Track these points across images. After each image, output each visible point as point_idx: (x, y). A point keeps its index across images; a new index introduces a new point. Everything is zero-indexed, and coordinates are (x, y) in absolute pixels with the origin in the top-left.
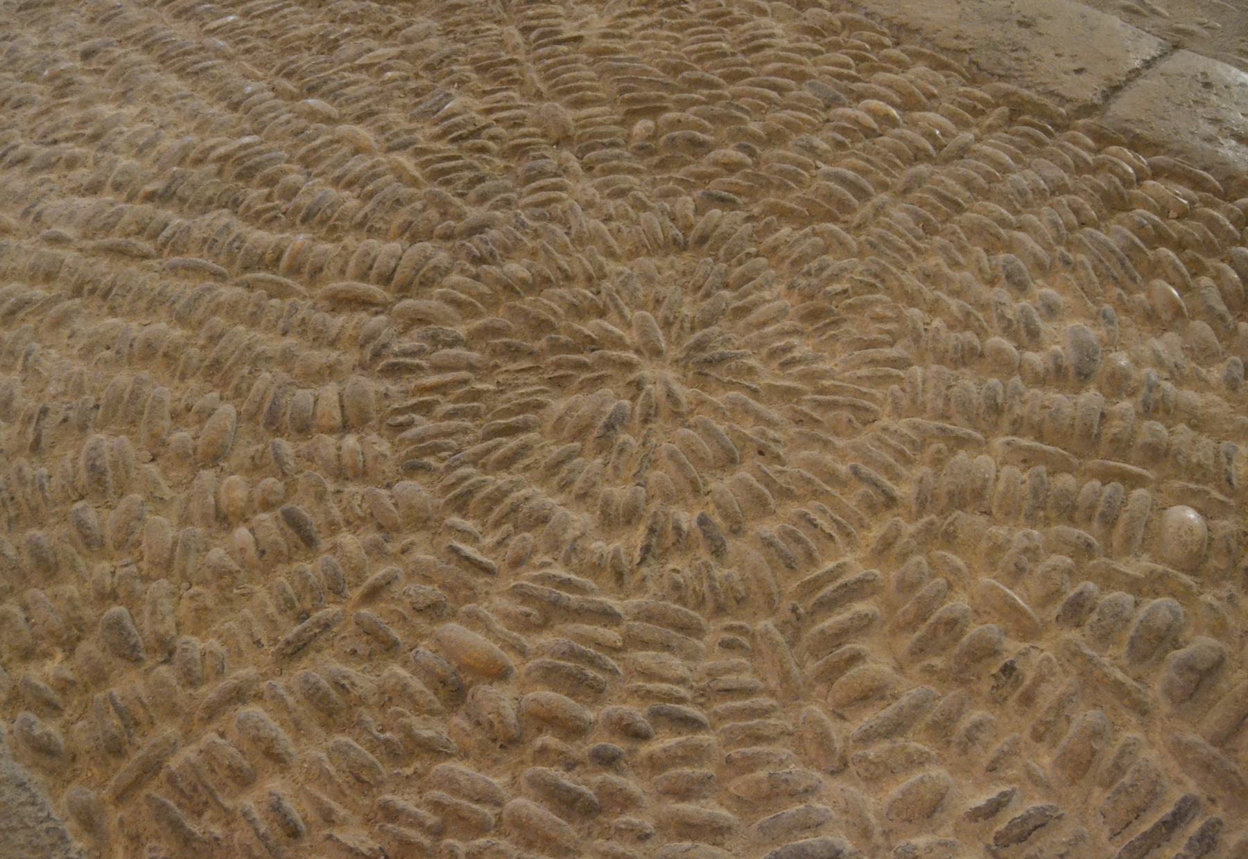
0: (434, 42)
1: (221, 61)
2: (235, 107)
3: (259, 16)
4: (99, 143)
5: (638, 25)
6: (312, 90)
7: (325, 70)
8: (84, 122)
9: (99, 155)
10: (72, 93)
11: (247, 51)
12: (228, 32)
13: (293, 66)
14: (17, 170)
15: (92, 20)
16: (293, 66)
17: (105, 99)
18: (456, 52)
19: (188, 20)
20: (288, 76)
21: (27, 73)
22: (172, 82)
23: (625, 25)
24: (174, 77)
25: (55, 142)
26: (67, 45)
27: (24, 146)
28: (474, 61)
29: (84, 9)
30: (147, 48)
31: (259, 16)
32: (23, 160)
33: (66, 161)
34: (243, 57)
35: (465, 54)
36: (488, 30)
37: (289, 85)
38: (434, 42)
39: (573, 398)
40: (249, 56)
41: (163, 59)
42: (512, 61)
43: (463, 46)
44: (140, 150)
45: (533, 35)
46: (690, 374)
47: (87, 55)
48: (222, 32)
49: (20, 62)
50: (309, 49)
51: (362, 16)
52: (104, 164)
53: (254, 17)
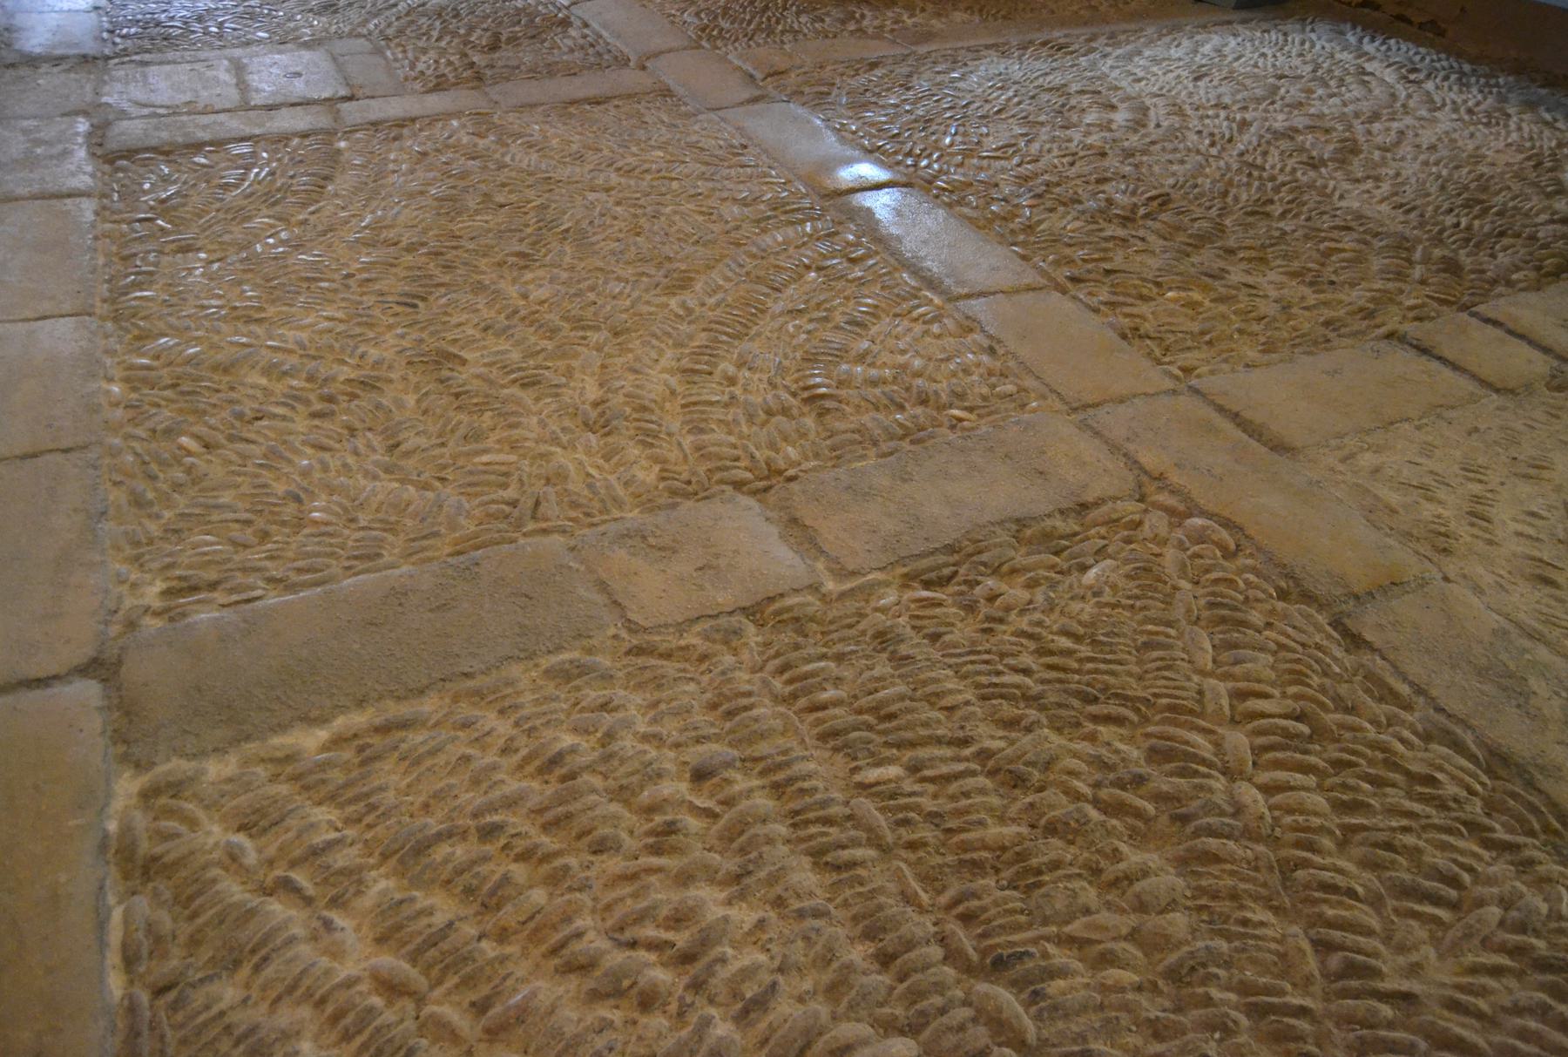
0: (1178, 922)
1: (871, 853)
2: (885, 960)
3: (932, 780)
4: (560, 771)
5: (1108, 233)
6: (998, 965)
7: (1018, 928)
8: (678, 920)
9: (688, 1000)
10: (674, 850)
11: (912, 846)
12: (885, 794)
13: (975, 903)
14: (573, 982)
15: (713, 706)
16: (975, 903)
17: (712, 879)
18: (1214, 956)
19: (836, 750)
20: (967, 919)
21: (621, 787)
22: (805, 876)
23: (1483, 992)
24: (806, 861)
25: (633, 945)
26: (677, 745)
27: (594, 941)
28: (1244, 989)
29: (706, 678)
30: (778, 789)
31: (932, 780)
32: (583, 967)
33: (641, 993)
34: (903, 853)
35: (1228, 965)
36: (1262, 924)
37: (965, 939)
38: (1178, 922)
39: (524, 784)
40: (912, 856)
41: (797, 819)
42: (1302, 1012)
43: (1223, 946)
44: (746, 1012)
45: (1335, 961)
46: (754, 547)
47: (700, 775)
48: (877, 794)
49: (616, 763)
50: (997, 871)
51: (1076, 832)
52: (693, 1018)
53: (924, 780)
